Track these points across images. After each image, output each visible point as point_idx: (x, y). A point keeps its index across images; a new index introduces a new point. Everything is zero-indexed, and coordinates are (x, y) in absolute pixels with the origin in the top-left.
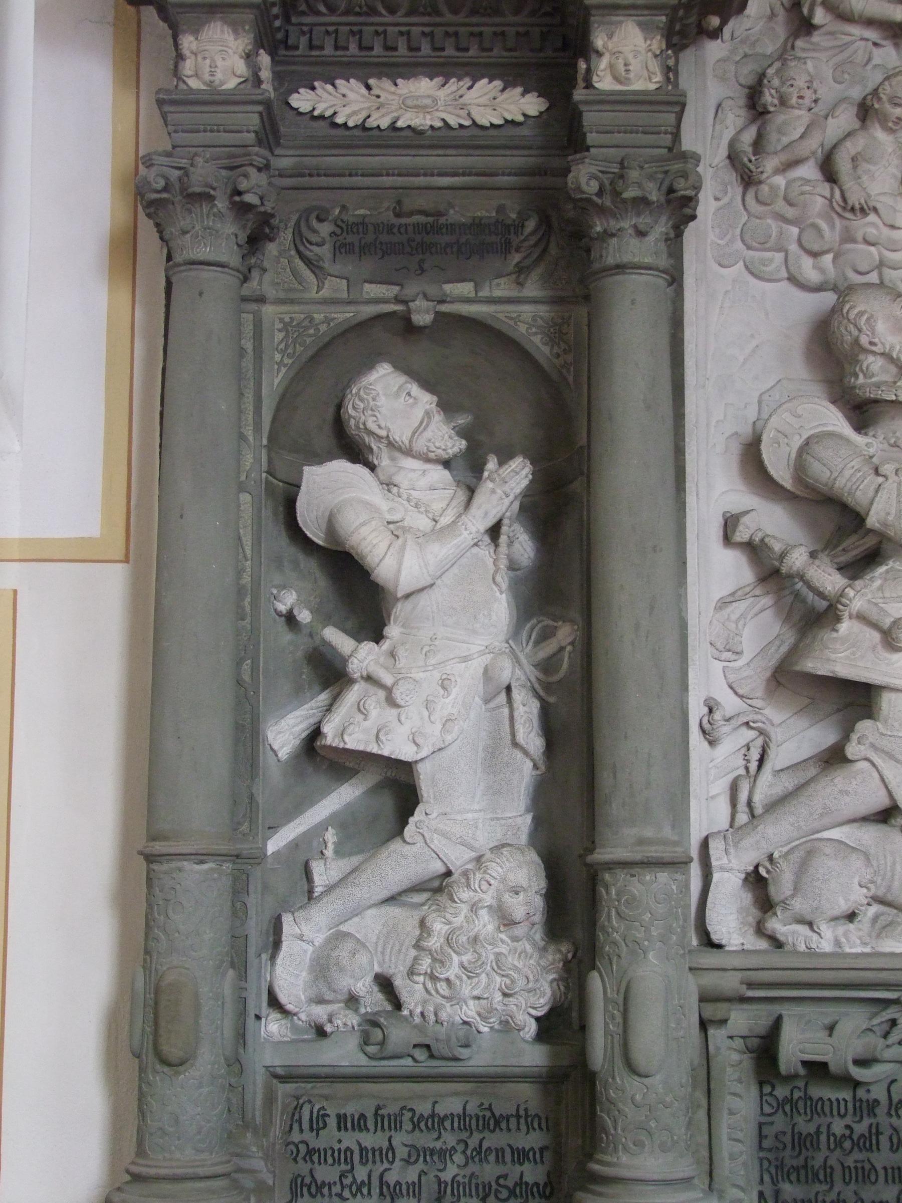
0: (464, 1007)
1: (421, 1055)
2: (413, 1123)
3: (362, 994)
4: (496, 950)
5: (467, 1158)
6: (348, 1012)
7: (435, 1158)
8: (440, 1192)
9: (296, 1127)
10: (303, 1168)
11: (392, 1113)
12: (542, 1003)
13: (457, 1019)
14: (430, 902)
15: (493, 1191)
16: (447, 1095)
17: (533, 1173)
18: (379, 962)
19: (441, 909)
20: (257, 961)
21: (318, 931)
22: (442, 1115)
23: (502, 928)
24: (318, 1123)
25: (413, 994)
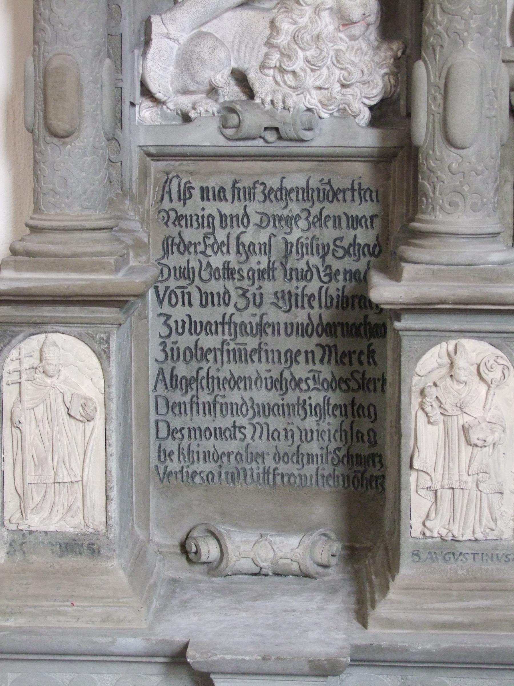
0: (308, 96)
1: (271, 136)
2: (265, 195)
3: (220, 84)
4: (336, 47)
5: (309, 224)
6: (209, 101)
7: (283, 223)
8: (287, 250)
9: (166, 196)
10: (173, 231)
11: (246, 186)
12: (375, 92)
13: (302, 105)
14: (279, 6)
15: (331, 251)
16: (293, 172)
17: (365, 236)
18: (235, 59)
19: (288, 11)
20: (131, 55)
21: (183, 30)
22: (289, 188)
23: (341, 28)
24: (185, 194)
25: (264, 85)
